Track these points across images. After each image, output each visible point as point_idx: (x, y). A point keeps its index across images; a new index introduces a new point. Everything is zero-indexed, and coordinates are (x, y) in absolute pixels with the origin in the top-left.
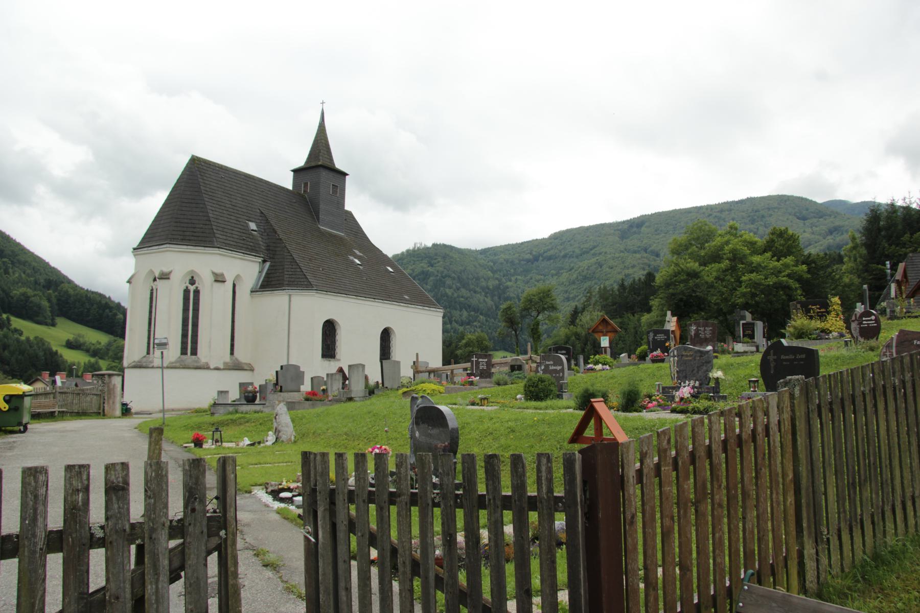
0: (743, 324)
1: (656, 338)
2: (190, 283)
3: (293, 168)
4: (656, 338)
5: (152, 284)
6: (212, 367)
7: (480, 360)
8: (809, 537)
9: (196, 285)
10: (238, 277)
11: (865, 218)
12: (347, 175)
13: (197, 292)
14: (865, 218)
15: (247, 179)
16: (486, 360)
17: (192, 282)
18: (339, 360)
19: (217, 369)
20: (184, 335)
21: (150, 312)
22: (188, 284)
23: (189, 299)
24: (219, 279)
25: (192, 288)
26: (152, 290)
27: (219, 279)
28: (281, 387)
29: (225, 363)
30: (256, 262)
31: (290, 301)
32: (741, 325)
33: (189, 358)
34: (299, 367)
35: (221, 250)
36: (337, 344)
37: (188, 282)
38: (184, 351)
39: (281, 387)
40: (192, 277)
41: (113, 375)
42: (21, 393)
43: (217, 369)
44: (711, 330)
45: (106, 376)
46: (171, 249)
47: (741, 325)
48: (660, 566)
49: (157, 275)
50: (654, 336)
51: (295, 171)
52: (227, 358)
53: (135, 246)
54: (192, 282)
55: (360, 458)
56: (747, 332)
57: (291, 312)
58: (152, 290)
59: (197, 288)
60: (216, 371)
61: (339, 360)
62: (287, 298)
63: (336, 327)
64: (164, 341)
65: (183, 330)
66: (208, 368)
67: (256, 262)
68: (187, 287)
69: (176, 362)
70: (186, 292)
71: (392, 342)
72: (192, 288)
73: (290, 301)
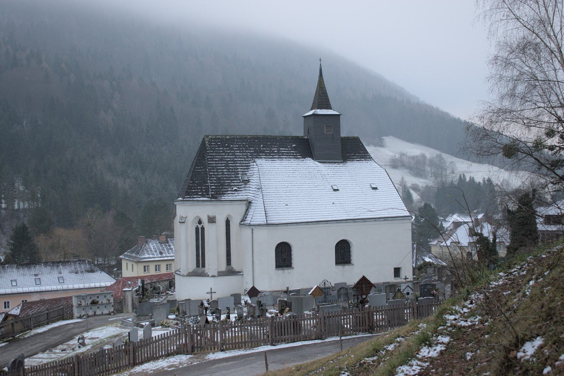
2: (198, 223)
6: (210, 275)
8: (30, 332)
11: (401, 327)
13: (203, 229)
14: (401, 327)
15: (298, 327)
23: (202, 240)
24: (212, 220)
25: (200, 226)
27: (212, 220)
31: (252, 233)
33: (200, 269)
37: (197, 223)
38: (198, 266)
43: (213, 276)
48: (199, 340)
57: (254, 240)
60: (213, 278)
62: (250, 231)
63: (291, 245)
65: (196, 252)
66: (208, 276)
68: (197, 226)
69: (192, 273)
70: (197, 229)
72: (200, 226)
73: (252, 233)
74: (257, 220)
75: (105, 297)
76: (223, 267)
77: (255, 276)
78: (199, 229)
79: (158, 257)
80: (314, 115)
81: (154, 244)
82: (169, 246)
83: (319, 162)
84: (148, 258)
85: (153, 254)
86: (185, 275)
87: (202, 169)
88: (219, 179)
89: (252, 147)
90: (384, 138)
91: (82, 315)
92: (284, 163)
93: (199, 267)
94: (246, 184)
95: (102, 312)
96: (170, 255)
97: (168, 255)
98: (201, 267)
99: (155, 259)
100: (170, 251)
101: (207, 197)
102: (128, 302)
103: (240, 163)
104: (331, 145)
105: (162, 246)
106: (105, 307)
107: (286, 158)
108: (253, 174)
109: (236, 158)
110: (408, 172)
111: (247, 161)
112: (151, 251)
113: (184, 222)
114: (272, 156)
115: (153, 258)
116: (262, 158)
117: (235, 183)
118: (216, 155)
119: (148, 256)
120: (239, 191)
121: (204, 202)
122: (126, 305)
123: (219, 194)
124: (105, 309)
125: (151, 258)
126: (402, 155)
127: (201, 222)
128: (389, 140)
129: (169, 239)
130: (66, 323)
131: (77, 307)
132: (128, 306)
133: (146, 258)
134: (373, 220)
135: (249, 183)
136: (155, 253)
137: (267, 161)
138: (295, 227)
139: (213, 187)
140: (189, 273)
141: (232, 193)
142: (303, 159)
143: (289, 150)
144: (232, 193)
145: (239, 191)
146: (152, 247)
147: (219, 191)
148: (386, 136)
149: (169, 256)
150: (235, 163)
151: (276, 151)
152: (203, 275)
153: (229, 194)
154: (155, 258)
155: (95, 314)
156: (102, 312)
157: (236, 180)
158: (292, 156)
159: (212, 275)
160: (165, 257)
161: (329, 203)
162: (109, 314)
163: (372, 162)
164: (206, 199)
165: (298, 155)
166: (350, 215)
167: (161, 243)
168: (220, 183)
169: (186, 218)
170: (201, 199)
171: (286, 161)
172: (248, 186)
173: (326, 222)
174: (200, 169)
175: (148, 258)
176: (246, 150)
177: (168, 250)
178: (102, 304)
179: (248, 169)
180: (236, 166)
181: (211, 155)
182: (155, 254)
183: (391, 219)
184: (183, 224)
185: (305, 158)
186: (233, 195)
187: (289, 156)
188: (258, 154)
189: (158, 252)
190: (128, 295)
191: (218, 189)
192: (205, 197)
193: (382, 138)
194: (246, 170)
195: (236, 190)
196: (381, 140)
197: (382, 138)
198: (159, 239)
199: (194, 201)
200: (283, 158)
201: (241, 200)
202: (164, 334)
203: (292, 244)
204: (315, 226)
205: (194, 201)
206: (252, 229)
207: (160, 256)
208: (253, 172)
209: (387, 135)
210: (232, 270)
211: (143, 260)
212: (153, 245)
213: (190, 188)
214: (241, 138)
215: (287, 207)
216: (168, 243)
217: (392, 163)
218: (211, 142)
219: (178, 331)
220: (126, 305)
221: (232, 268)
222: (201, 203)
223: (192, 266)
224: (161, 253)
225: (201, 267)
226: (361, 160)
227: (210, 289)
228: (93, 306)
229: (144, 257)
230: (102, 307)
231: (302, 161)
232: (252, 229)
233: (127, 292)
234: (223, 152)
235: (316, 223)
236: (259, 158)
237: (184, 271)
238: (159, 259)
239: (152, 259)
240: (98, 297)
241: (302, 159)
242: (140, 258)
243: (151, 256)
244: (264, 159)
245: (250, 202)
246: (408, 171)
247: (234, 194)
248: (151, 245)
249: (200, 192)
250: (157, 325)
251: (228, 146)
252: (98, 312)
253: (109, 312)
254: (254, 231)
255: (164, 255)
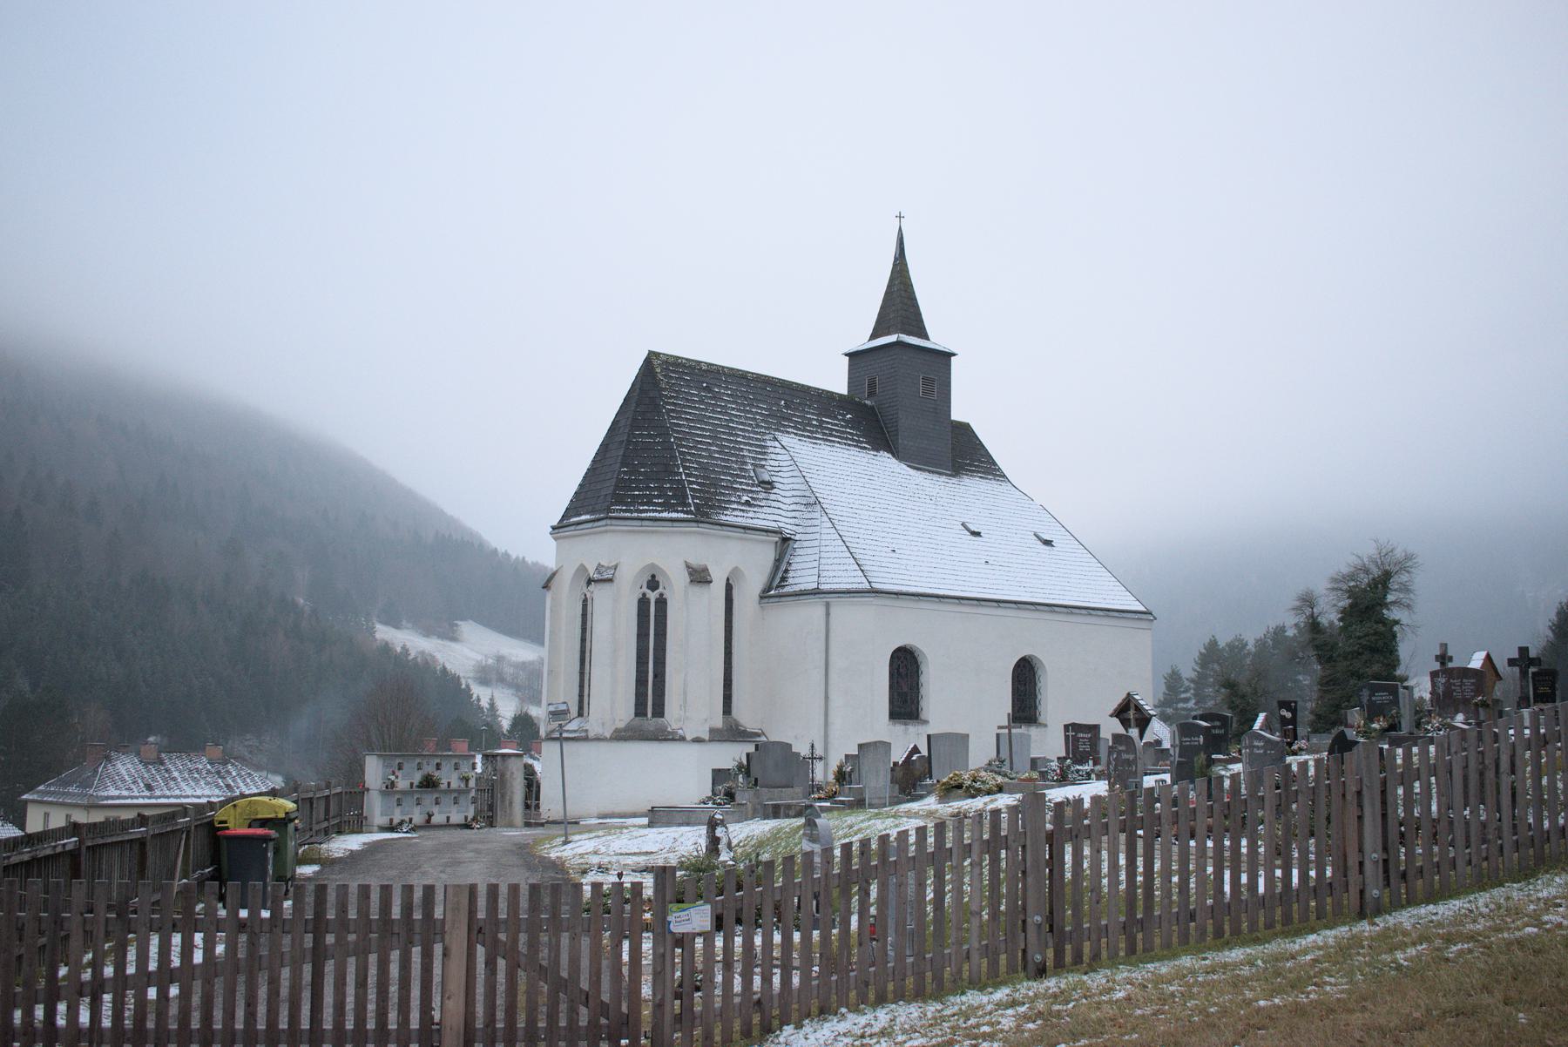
0: (1533, 673)
1: (1374, 698)
2: (648, 587)
3: (847, 350)
4: (1374, 698)
5: (585, 590)
6: (689, 738)
7: (1081, 735)
9: (661, 590)
10: (736, 570)
12: (954, 355)
13: (662, 603)
16: (1089, 735)
17: (653, 584)
18: (926, 722)
19: (698, 740)
20: (641, 681)
21: (583, 640)
22: (645, 589)
25: (653, 596)
26: (585, 600)
27: (699, 577)
28: (756, 780)
29: (712, 731)
30: (769, 542)
31: (828, 614)
32: (1530, 675)
33: (651, 723)
34: (789, 746)
35: (700, 525)
36: (923, 691)
38: (640, 710)
39: (756, 780)
40: (653, 576)
41: (509, 755)
42: (282, 815)
43: (698, 740)
44: (1473, 684)
45: (499, 758)
46: (612, 528)
47: (1530, 675)
49: (592, 573)
50: (1370, 696)
51: (853, 356)
52: (718, 721)
53: (555, 523)
54: (653, 584)
55: (386, 890)
56: (1541, 690)
58: (585, 600)
59: (661, 595)
60: (696, 746)
61: (926, 722)
62: (821, 610)
63: (919, 659)
64: (564, 707)
66: (683, 739)
67: (769, 542)
68: (644, 595)
69: (626, 729)
70: (643, 603)
71: (1039, 685)
72: (653, 596)
73: (828, 614)
74: (836, 580)
75: (456, 767)
76: (718, 721)
77: (831, 739)
78: (649, 603)
79: (143, 797)
80: (899, 343)
81: (129, 766)
82: (167, 771)
83: (908, 466)
84: (118, 797)
85: (129, 789)
86: (608, 735)
87: (656, 436)
88: (703, 467)
89: (764, 402)
90: (459, 623)
91: (396, 821)
92: (840, 455)
93: (646, 715)
94: (767, 491)
95: (448, 818)
96: (173, 794)
97: (168, 793)
98: (650, 715)
99: (135, 801)
100: (172, 784)
101: (682, 511)
102: (512, 792)
103: (744, 437)
104: (931, 426)
105: (149, 771)
106: (437, 803)
107: (839, 442)
108: (779, 469)
109: (733, 422)
110: (513, 695)
111: (756, 433)
112: (124, 781)
113: (610, 580)
114: (809, 431)
115: (132, 798)
116: (788, 432)
117: (741, 483)
118: (684, 406)
119: (117, 793)
120: (755, 506)
121: (675, 524)
122: (507, 802)
123: (711, 507)
124: (454, 809)
125: (126, 798)
126: (500, 659)
127: (658, 582)
128: (467, 628)
129: (163, 755)
130: (391, 837)
131: (383, 793)
132: (511, 803)
133: (112, 798)
134: (1083, 612)
135: (775, 490)
136: (133, 786)
137: (800, 443)
138: (936, 606)
139: (694, 486)
140: (617, 731)
141: (741, 510)
142: (876, 453)
143: (842, 426)
144: (741, 510)
145: (755, 506)
146: (123, 772)
147: (711, 499)
148: (461, 620)
149: (172, 796)
150: (731, 435)
151: (814, 423)
152: (664, 736)
153: (734, 509)
154: (137, 798)
155: (428, 821)
156: (448, 818)
157: (744, 477)
158: (850, 440)
159: (695, 736)
160: (160, 797)
161: (978, 561)
162: (467, 826)
163: (1005, 487)
164: (681, 515)
165: (862, 442)
166: (1036, 595)
167: (146, 764)
168: (708, 478)
169: (615, 567)
170: (665, 515)
171: (839, 450)
172: (773, 497)
173: (995, 604)
174: (650, 436)
175: (118, 797)
176: (752, 406)
177: (164, 779)
178: (449, 791)
179: (765, 453)
180: (737, 442)
181: (674, 404)
182: (135, 790)
183: (1133, 616)
184: (606, 586)
185: (878, 451)
186: (745, 515)
187: (844, 439)
188: (780, 421)
189: (142, 785)
190: (514, 770)
191: (708, 492)
192: (678, 512)
193: (456, 622)
194: (759, 456)
195: (747, 503)
196: (453, 626)
197: (456, 622)
198: (138, 754)
199: (642, 519)
200: (834, 441)
201: (767, 531)
202: (903, 835)
203: (925, 650)
204: (974, 610)
205: (642, 519)
206: (828, 605)
207: (147, 793)
208: (776, 463)
209: (463, 619)
210: (737, 728)
211: (105, 802)
212: (125, 766)
213: (622, 485)
214: (734, 375)
215: (893, 555)
216: (162, 763)
217: (479, 675)
218: (667, 369)
219: (950, 835)
220: (507, 802)
221: (737, 724)
222: (667, 527)
223: (624, 711)
224: (149, 787)
225: (650, 715)
226: (987, 478)
227: (809, 746)
228: (426, 792)
229: (106, 794)
230: (447, 800)
231: (875, 458)
232: (828, 605)
233: (513, 758)
234: (701, 402)
235: (975, 602)
236: (783, 432)
237: (603, 724)
238: (147, 801)
239: (129, 801)
240: (438, 766)
241: (872, 453)
242: (97, 797)
243: (125, 793)
244: (793, 436)
245: (785, 540)
246: (511, 691)
247: (747, 511)
248: (119, 765)
249: (658, 497)
250: (869, 805)
251: (708, 389)
252: (438, 819)
253: (466, 818)
254: (833, 610)
255: (158, 793)
